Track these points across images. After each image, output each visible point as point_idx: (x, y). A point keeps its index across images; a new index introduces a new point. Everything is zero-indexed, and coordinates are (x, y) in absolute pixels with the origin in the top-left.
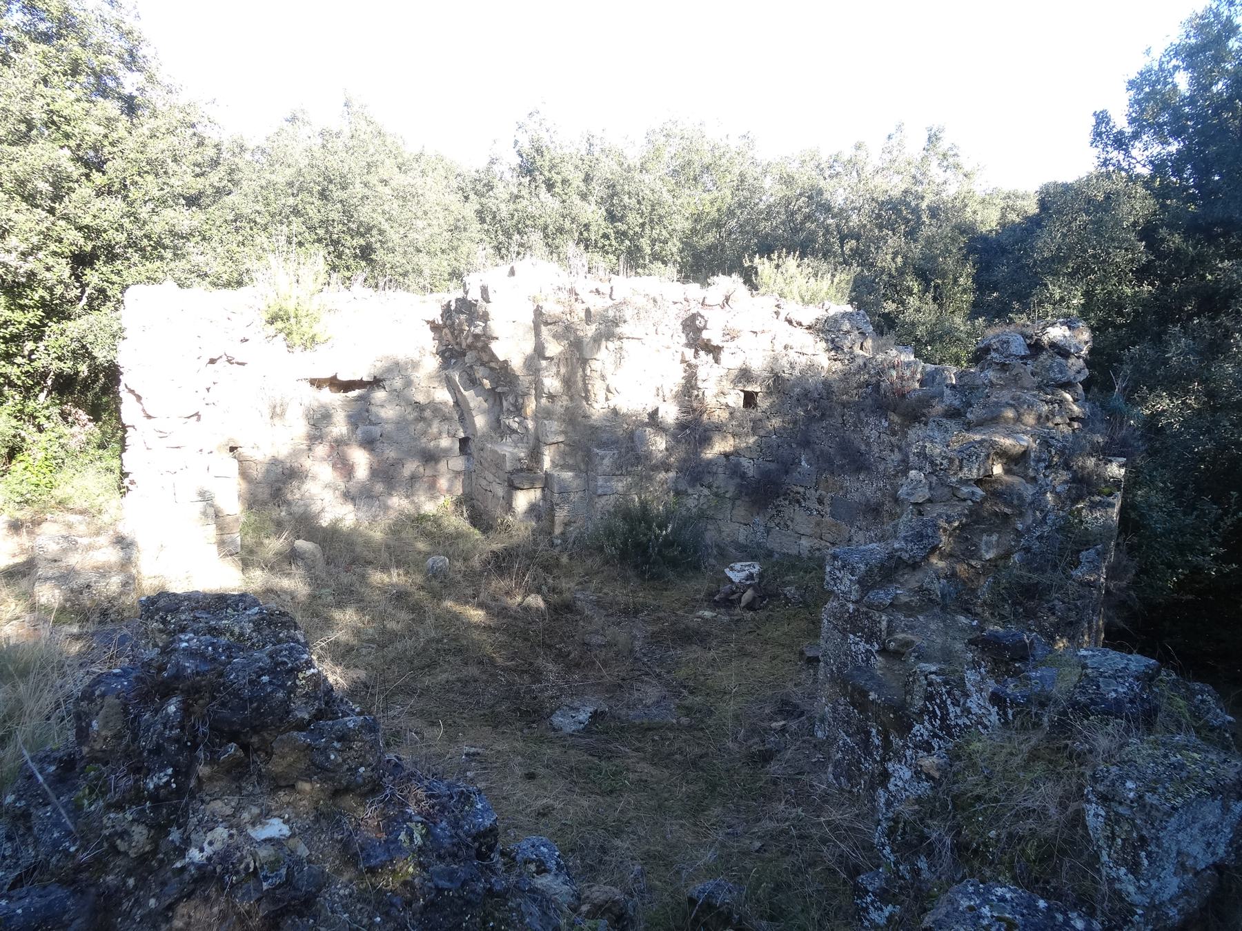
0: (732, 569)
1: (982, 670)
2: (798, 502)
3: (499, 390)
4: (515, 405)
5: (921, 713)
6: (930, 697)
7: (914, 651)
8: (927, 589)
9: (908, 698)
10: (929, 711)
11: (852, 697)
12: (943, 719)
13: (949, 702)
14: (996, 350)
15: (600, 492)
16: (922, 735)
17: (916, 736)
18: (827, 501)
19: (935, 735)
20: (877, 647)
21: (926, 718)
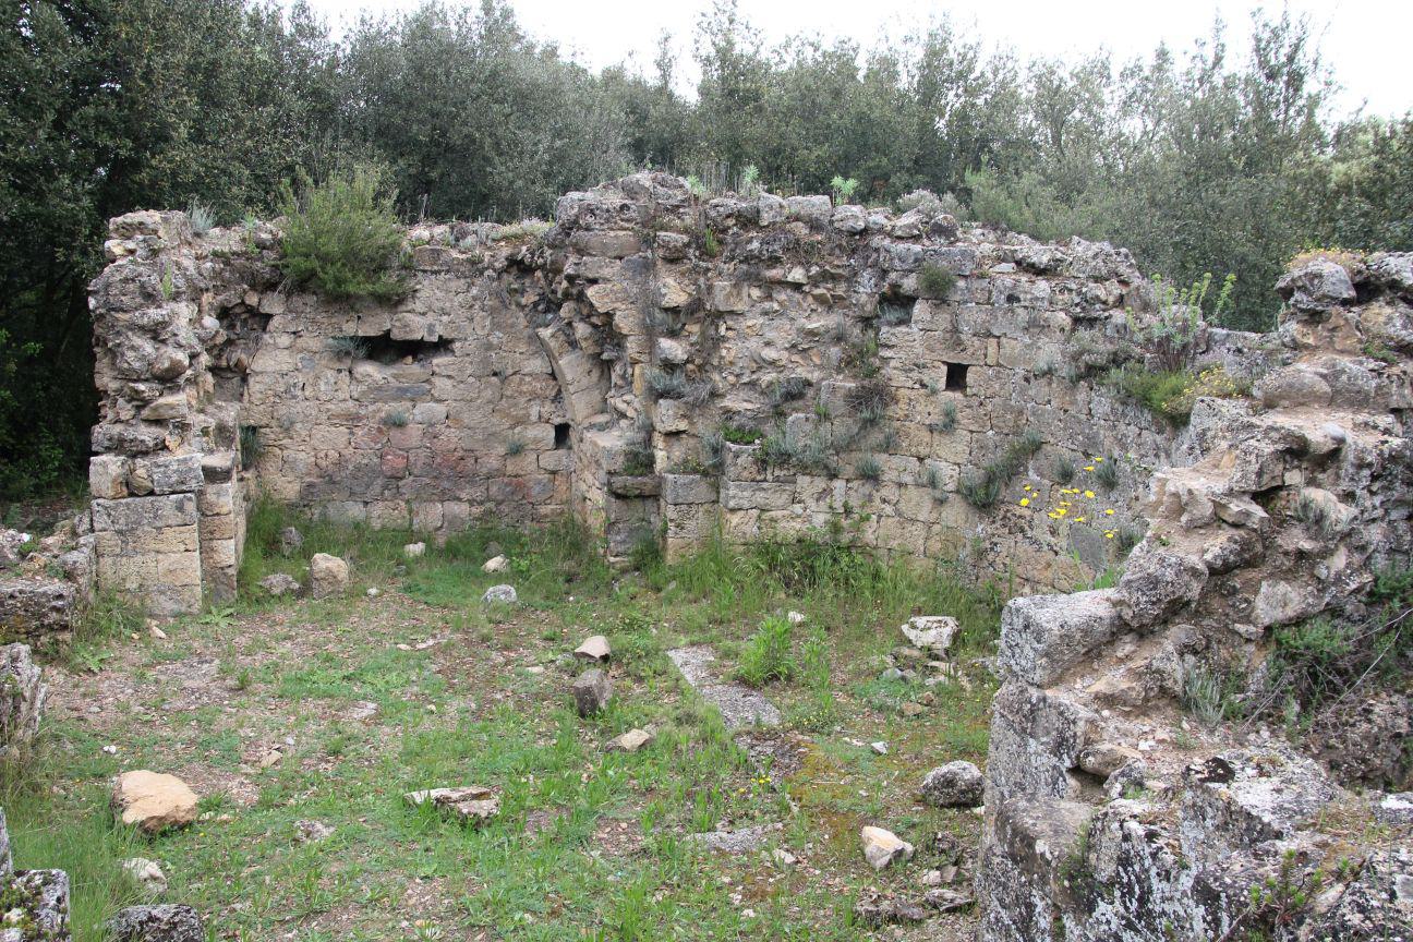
0: (913, 627)
1: (1209, 823)
2: (1022, 530)
3: (605, 356)
4: (623, 377)
5: (1110, 884)
6: (1124, 861)
7: (1123, 774)
8: (1158, 671)
9: (1093, 856)
10: (1122, 885)
11: (1011, 845)
12: (1143, 901)
13: (1153, 871)
14: (1303, 289)
15: (732, 504)
16: (1108, 922)
17: (1098, 922)
18: (1063, 530)
19: (1130, 926)
20: (1068, 763)
21: (1117, 893)
